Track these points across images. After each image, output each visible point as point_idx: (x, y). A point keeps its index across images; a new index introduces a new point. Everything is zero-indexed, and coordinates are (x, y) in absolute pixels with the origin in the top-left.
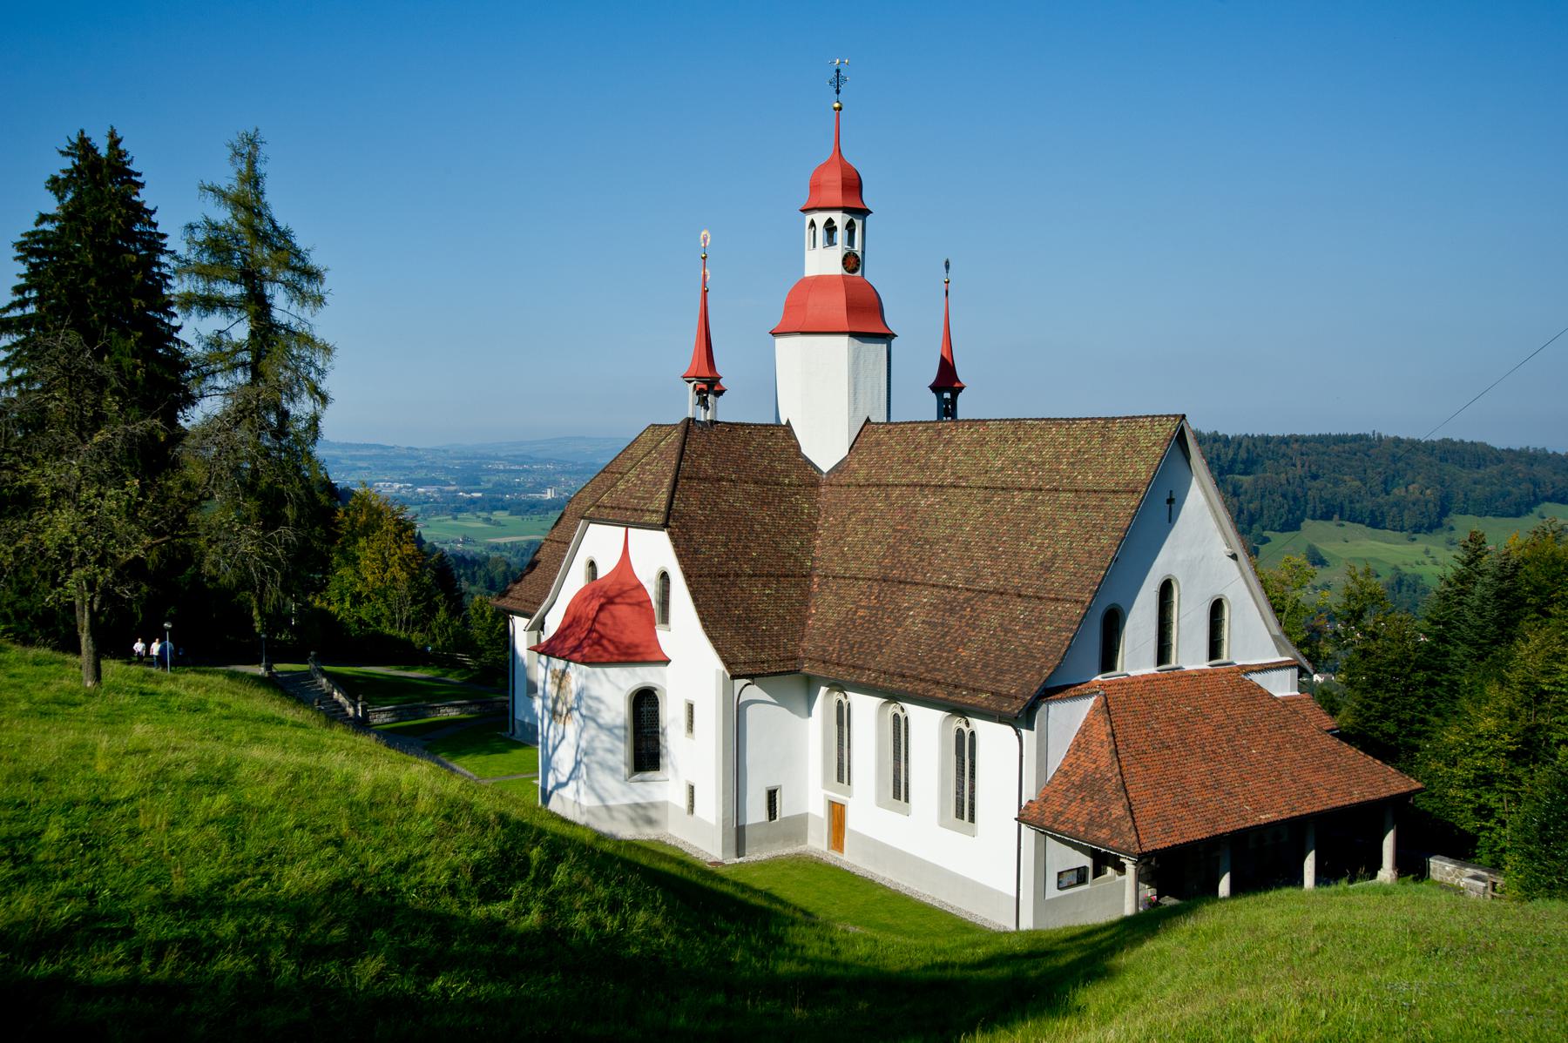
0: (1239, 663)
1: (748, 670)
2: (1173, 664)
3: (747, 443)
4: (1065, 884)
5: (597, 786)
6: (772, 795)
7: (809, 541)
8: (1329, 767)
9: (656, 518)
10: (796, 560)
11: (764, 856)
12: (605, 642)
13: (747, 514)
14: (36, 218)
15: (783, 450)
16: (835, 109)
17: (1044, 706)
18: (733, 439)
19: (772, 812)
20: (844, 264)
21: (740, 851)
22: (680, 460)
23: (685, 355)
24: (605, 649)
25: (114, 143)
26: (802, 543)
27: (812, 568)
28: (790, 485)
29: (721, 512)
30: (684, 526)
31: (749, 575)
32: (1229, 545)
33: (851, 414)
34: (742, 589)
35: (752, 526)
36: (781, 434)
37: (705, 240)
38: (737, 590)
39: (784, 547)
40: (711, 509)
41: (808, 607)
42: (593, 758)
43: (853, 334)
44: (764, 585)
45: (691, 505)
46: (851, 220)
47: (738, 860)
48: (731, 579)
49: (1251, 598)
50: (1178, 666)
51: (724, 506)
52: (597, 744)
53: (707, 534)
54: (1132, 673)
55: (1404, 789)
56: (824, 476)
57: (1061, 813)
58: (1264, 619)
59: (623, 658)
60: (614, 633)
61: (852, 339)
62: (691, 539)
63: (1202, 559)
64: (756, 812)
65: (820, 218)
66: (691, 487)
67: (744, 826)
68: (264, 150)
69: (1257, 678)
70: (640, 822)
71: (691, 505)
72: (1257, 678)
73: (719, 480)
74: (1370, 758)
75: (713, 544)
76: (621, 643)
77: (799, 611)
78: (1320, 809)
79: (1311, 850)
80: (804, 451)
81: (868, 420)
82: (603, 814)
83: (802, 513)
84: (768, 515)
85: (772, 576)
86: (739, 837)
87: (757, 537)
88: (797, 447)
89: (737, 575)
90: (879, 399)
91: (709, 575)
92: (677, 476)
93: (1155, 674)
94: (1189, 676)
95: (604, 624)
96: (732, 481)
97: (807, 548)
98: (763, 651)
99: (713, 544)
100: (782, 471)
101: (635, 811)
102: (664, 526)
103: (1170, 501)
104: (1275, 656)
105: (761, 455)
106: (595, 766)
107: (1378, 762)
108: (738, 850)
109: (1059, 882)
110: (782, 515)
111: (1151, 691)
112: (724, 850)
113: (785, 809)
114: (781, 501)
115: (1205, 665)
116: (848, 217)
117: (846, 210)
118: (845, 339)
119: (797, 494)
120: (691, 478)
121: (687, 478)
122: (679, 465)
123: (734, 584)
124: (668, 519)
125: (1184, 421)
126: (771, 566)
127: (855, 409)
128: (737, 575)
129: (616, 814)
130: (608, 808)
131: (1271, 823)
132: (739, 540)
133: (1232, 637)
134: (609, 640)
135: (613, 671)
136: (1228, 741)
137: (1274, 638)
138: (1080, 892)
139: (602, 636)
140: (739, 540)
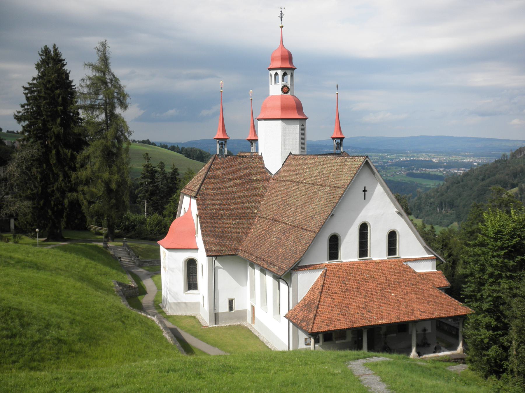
0: (403, 257)
1: (215, 253)
2: (368, 257)
4: (306, 343)
6: (231, 303)
7: (259, 202)
9: (194, 194)
10: (251, 210)
13: (233, 192)
14: (32, 78)
15: (256, 166)
18: (235, 162)
19: (231, 307)
21: (216, 321)
22: (208, 171)
26: (255, 203)
27: (257, 213)
28: (257, 180)
29: (221, 192)
30: (203, 197)
31: (228, 217)
32: (397, 208)
34: (223, 222)
35: (234, 197)
36: (257, 159)
37: (222, 84)
38: (221, 222)
39: (247, 205)
40: (217, 190)
41: (251, 229)
44: (233, 220)
45: (209, 189)
47: (214, 326)
51: (223, 189)
53: (213, 200)
54: (344, 261)
56: (273, 176)
57: (297, 315)
62: (205, 202)
64: (223, 308)
65: (273, 72)
66: (210, 182)
69: (410, 264)
71: (209, 189)
72: (410, 264)
73: (223, 179)
74: (453, 299)
75: (214, 204)
77: (246, 231)
81: (291, 153)
83: (259, 191)
84: (243, 192)
86: (216, 317)
87: (235, 201)
88: (263, 164)
89: (222, 216)
92: (205, 177)
93: (356, 261)
94: (376, 263)
96: (229, 179)
97: (257, 205)
98: (224, 246)
99: (214, 204)
100: (254, 174)
102: (195, 197)
105: (246, 168)
107: (457, 301)
108: (215, 322)
109: (305, 342)
110: (249, 192)
111: (351, 268)
112: (210, 321)
113: (237, 307)
114: (250, 186)
120: (212, 178)
121: (209, 178)
122: (207, 173)
123: (220, 220)
124: (197, 195)
126: (238, 212)
128: (222, 216)
131: (383, 324)
132: (226, 203)
133: (400, 246)
136: (382, 290)
137: (425, 247)
140: (226, 203)
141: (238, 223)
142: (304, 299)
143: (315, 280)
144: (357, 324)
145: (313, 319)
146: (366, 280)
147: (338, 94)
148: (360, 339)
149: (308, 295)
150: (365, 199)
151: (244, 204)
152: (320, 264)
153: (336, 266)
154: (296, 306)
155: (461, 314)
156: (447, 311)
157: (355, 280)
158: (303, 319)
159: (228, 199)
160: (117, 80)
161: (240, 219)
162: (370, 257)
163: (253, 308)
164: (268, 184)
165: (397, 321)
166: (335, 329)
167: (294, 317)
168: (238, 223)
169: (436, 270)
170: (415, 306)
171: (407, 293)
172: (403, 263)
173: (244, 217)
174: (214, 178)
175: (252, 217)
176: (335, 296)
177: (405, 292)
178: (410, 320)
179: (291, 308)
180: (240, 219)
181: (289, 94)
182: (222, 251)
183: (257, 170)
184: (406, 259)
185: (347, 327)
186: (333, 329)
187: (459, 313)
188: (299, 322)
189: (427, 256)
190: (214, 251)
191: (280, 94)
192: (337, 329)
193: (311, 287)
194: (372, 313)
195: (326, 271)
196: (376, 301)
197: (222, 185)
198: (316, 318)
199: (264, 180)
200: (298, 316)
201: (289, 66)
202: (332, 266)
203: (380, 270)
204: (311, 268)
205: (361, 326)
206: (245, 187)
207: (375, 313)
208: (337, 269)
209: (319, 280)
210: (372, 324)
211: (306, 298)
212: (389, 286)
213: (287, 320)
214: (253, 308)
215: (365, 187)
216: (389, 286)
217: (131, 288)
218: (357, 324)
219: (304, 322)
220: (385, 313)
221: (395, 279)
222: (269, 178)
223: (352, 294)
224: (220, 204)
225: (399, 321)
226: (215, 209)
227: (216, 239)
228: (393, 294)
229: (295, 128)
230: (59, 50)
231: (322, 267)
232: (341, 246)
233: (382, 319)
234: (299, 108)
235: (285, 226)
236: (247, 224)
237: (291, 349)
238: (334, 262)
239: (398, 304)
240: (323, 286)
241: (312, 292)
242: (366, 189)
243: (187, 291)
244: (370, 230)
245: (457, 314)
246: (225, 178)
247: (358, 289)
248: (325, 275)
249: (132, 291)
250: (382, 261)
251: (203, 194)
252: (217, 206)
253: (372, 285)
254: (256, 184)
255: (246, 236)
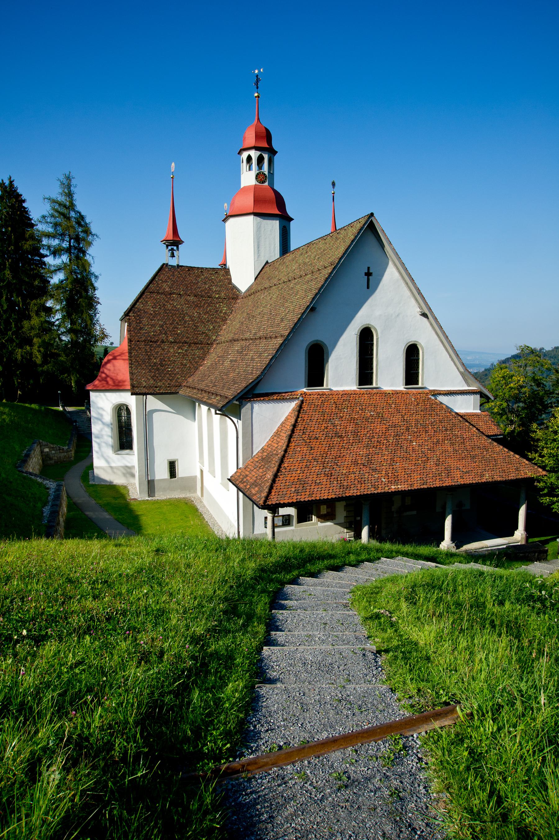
0: (431, 388)
3: (199, 276)
5: (105, 455)
6: (172, 465)
7: (219, 326)
8: (473, 457)
10: (207, 335)
11: (164, 498)
12: (108, 379)
15: (220, 281)
16: (256, 97)
17: (249, 405)
19: (173, 473)
20: (256, 178)
23: (166, 232)
24: (107, 383)
25: (11, 182)
28: (219, 298)
29: (165, 310)
31: (171, 342)
32: (420, 307)
33: (256, 259)
35: (183, 318)
39: (201, 328)
42: (102, 440)
43: (256, 214)
44: (179, 348)
46: (261, 155)
47: (147, 498)
48: (159, 343)
49: (442, 345)
50: (377, 386)
51: (169, 307)
52: (104, 433)
54: (334, 389)
55: (529, 474)
58: (452, 360)
59: (114, 388)
60: (113, 375)
61: (255, 217)
62: (140, 322)
63: (398, 315)
67: (153, 481)
68: (73, 182)
69: (442, 399)
70: (128, 475)
74: (512, 453)
75: (153, 326)
76: (117, 380)
78: (450, 484)
79: (449, 514)
80: (233, 281)
82: (109, 470)
83: (221, 312)
85: (186, 343)
87: (185, 322)
88: (230, 280)
89: (163, 342)
90: (274, 251)
91: (145, 341)
93: (354, 391)
94: (386, 394)
95: (109, 370)
96: (180, 294)
97: (216, 330)
101: (125, 470)
103: (368, 274)
104: (463, 386)
106: (103, 444)
107: (517, 456)
110: (207, 313)
113: (181, 472)
114: (209, 305)
115: (401, 387)
116: (258, 153)
117: (256, 148)
118: (251, 218)
119: (221, 302)
120: (154, 292)
123: (159, 346)
125: (373, 218)
126: (187, 338)
127: (259, 256)
128: (163, 342)
129: (115, 470)
130: (111, 467)
133: (425, 370)
134: (111, 378)
135: (109, 395)
137: (462, 374)
138: (286, 531)
139: (107, 376)
141: (186, 351)
142: (263, 450)
143: (283, 419)
144: (352, 491)
145: (270, 481)
146: (369, 420)
147: (334, 193)
148: (359, 518)
149: (270, 442)
150: (368, 288)
151: (197, 327)
152: (291, 392)
153: (319, 396)
154: (249, 463)
155: (526, 476)
156: (504, 471)
157: (352, 420)
158: (255, 481)
159: (174, 320)
160: (82, 217)
161: (189, 346)
162: (377, 384)
163: (202, 471)
164: (234, 304)
165: (422, 487)
166: (310, 499)
167: (242, 479)
168: (186, 351)
169: (479, 411)
170: (452, 463)
171: (438, 442)
172: (430, 396)
173: (195, 344)
174: (158, 293)
175: (208, 344)
176: (314, 443)
177: (435, 440)
178: (444, 485)
179: (241, 465)
180: (189, 346)
181: (266, 184)
182: (156, 387)
183: (221, 286)
184: (434, 390)
185: (334, 496)
186: (306, 499)
187: (522, 475)
188: (248, 487)
189: (466, 388)
190: (144, 387)
191: (254, 184)
192: (313, 498)
193: (275, 430)
194: (380, 472)
195: (302, 402)
196: (387, 453)
197: (167, 302)
198: (277, 480)
199: (229, 299)
200: (248, 478)
201: (266, 145)
202: (312, 396)
203: (393, 406)
204: (275, 398)
205: (359, 494)
206: (201, 307)
207: (384, 472)
208: (320, 401)
209: (289, 417)
210: (379, 491)
211: (266, 447)
212: (408, 429)
213: (235, 489)
214: (202, 471)
215: (369, 268)
216: (408, 429)
217: (61, 451)
218: (352, 491)
219: (256, 486)
220: (402, 475)
221: (417, 420)
222: (237, 297)
223: (345, 442)
224: (162, 326)
225: (425, 487)
226: (153, 332)
227: (150, 371)
228: (414, 444)
229: (275, 225)
230: (16, 184)
231: (294, 397)
232: (327, 361)
233: (396, 483)
234: (280, 202)
235: (243, 343)
236: (197, 352)
237: (242, 536)
238: (317, 390)
239: (423, 459)
240: (294, 426)
241: (275, 438)
242: (371, 272)
243: (118, 451)
244: (377, 339)
245: (520, 477)
246: (174, 293)
247: (356, 433)
248: (300, 407)
249: (63, 454)
250: (396, 393)
251: (139, 312)
252: (158, 328)
253: (379, 428)
254: (217, 303)
255: (197, 369)
